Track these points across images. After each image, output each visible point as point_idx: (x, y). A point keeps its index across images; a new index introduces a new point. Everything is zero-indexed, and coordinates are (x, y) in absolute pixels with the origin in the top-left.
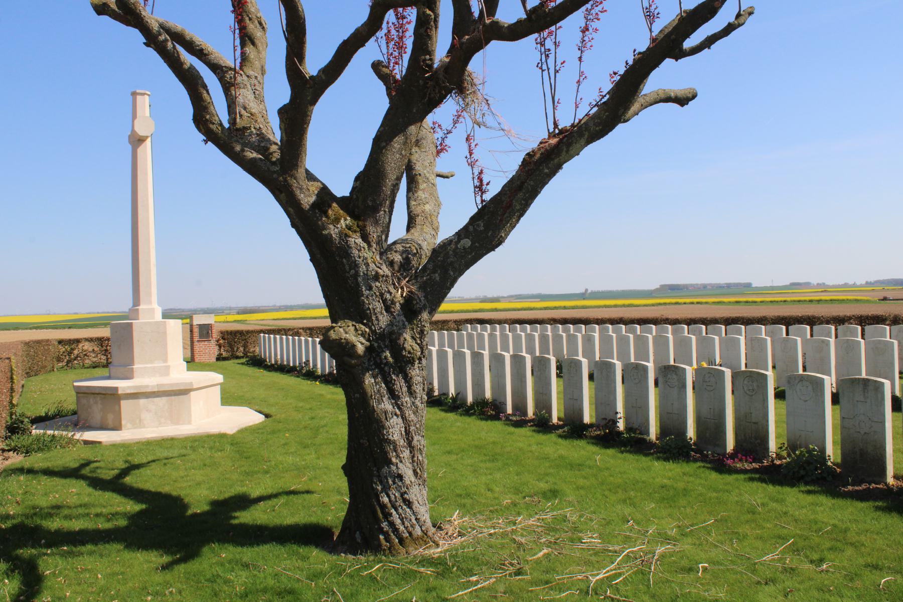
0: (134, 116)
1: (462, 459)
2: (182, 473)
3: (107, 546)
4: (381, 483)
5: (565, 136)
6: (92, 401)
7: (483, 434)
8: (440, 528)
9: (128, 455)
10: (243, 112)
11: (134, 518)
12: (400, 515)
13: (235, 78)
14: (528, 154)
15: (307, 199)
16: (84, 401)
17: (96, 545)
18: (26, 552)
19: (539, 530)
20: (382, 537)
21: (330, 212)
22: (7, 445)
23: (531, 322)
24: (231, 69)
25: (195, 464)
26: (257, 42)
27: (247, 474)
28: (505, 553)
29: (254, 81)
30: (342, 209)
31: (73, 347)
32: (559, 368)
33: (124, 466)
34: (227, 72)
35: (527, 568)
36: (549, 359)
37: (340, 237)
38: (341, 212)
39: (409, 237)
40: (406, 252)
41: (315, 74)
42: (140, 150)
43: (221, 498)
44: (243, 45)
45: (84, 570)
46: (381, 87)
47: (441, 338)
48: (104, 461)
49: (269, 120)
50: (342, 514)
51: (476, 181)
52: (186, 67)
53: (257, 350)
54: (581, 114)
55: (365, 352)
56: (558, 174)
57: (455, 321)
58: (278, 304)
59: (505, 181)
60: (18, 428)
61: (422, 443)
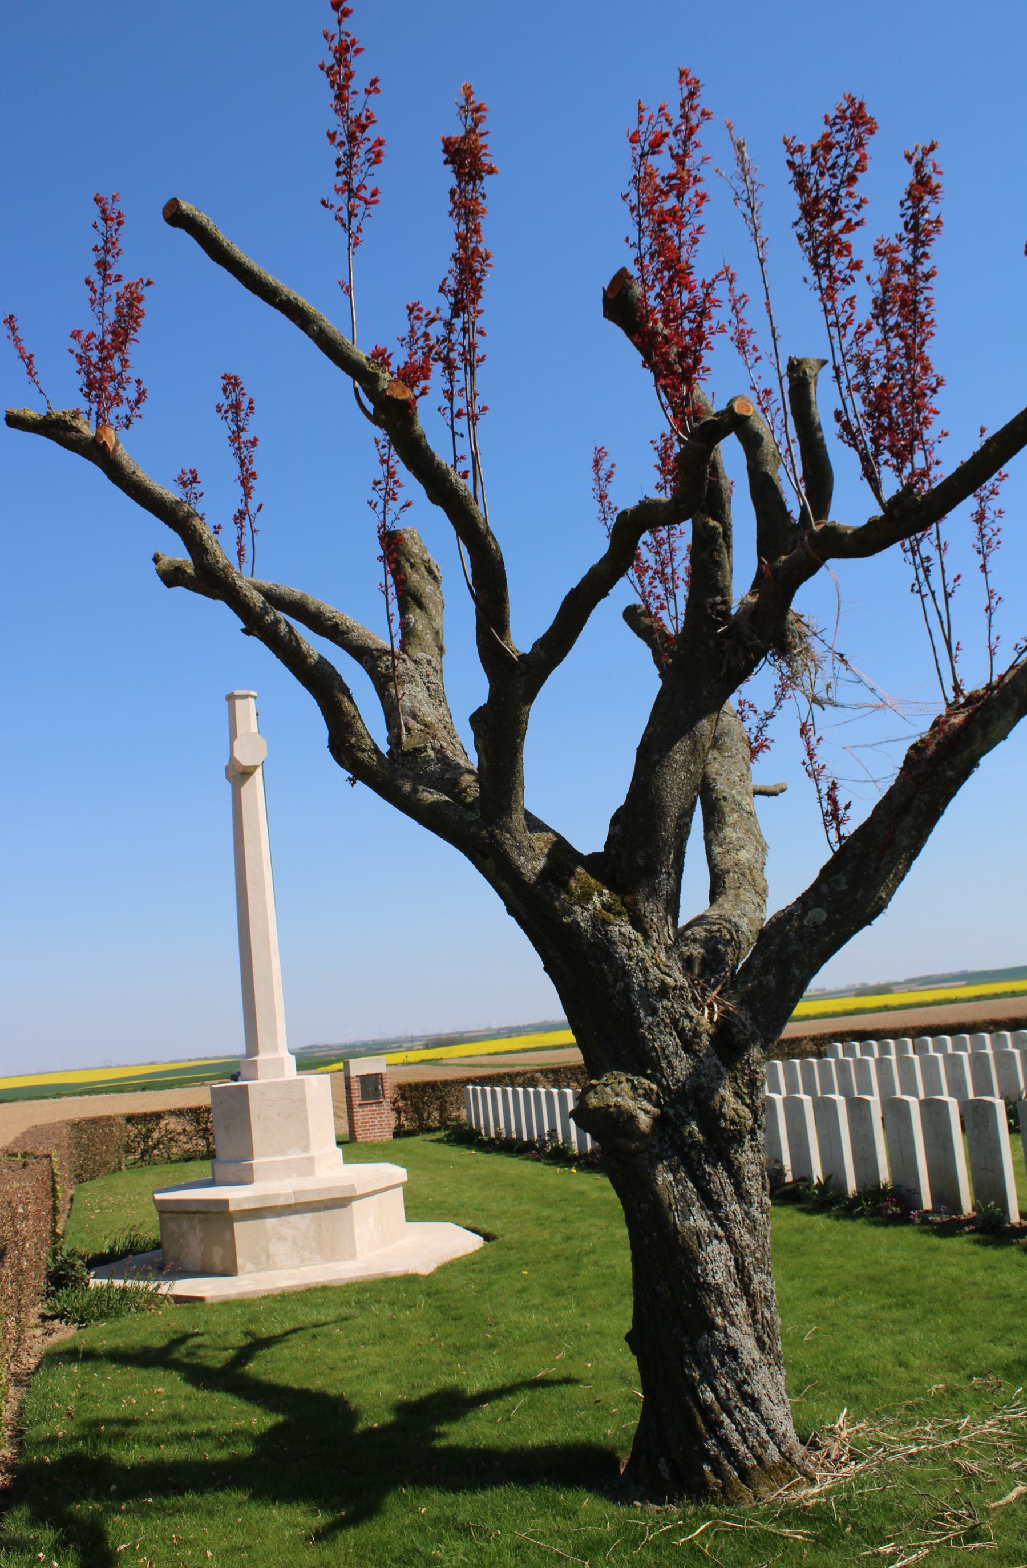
0: (233, 735)
1: (847, 1305)
2: (344, 1353)
3: (221, 1495)
4: (699, 1365)
5: (978, 708)
6: (185, 1226)
7: (882, 1254)
8: (814, 1446)
9: (250, 1321)
10: (412, 723)
11: (264, 1440)
12: (737, 1424)
13: (394, 667)
14: (914, 747)
15: (532, 865)
16: (172, 1226)
17: (202, 1493)
18: (84, 1508)
19: (1005, 1443)
20: (707, 1468)
21: (573, 883)
22: (50, 1308)
23: (954, 1030)
24: (386, 652)
25: (366, 1334)
26: (426, 602)
27: (458, 1350)
28: (942, 1495)
29: (426, 669)
30: (593, 876)
31: (150, 1126)
32: (1011, 1114)
33: (244, 1342)
34: (380, 658)
35: (987, 1525)
36: (992, 1105)
37: (594, 926)
38: (593, 881)
39: (714, 913)
40: (711, 943)
41: (528, 651)
42: (245, 790)
43: (415, 1398)
44: (403, 609)
45: (184, 1543)
46: (643, 651)
47: (790, 1072)
48: (209, 1333)
49: (457, 731)
50: (633, 1423)
51: (825, 803)
52: (312, 661)
53: (464, 1113)
54: (1002, 666)
55: (653, 1127)
56: (972, 777)
57: (813, 1039)
58: (495, 1026)
59: (878, 797)
60: (66, 1276)
61: (769, 1286)
